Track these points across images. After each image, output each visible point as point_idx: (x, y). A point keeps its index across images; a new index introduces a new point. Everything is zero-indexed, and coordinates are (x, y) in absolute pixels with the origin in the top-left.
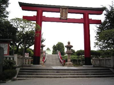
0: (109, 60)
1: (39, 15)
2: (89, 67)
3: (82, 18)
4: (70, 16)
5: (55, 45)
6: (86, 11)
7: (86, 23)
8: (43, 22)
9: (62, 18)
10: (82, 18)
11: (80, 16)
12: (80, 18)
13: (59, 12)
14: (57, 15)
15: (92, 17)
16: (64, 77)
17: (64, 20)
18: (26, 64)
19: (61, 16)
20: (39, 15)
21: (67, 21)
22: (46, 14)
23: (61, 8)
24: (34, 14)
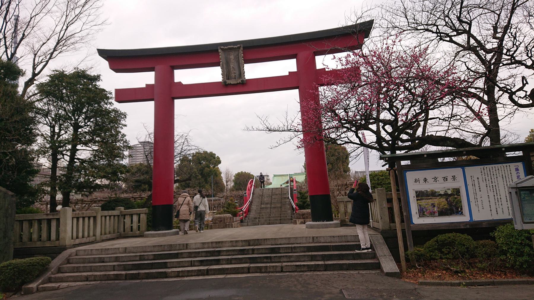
0: (110, 216)
1: (307, 66)
2: (116, 244)
3: (295, 69)
4: (253, 71)
5: (219, 166)
6: (303, 46)
7: (307, 81)
8: (176, 101)
9: (228, 82)
10: (295, 69)
11: (286, 67)
12: (144, 86)
13: (216, 64)
14: (213, 74)
15: (326, 62)
16: (148, 276)
17: (233, 85)
18: (31, 239)
19: (226, 74)
20: (307, 66)
21: (245, 89)
22: (184, 76)
23: (222, 49)
24: (145, 79)
